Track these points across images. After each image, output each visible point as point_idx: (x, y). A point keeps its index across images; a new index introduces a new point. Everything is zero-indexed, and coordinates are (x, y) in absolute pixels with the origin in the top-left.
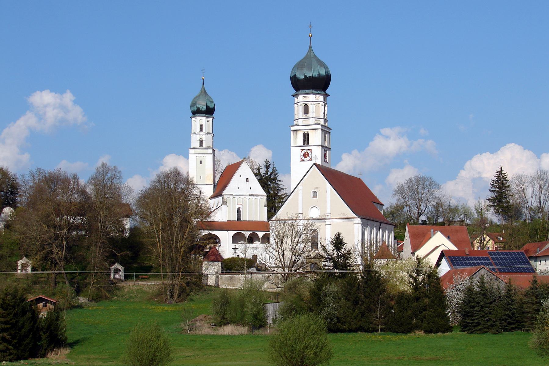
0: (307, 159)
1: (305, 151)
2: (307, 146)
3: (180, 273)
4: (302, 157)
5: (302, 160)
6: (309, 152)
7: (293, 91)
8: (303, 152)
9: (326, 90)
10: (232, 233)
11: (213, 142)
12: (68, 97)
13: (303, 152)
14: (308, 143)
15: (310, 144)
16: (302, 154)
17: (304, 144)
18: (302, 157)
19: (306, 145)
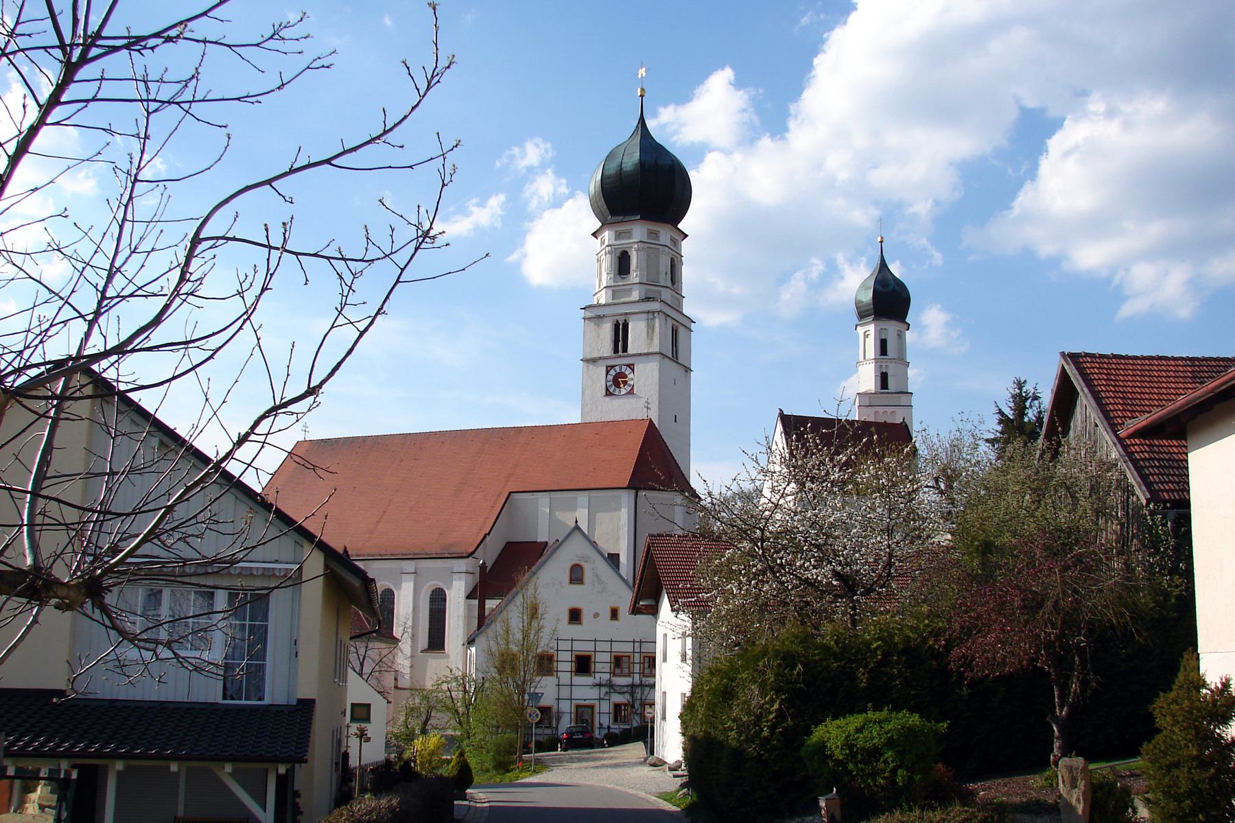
0: (623, 391)
1: (618, 369)
2: (624, 357)
3: (1058, 543)
4: (609, 384)
5: (608, 393)
6: (628, 371)
7: (857, 321)
8: (612, 372)
9: (169, 428)
10: (560, 541)
11: (405, 117)
12: (549, 145)
13: (612, 372)
14: (625, 349)
15: (631, 350)
16: (610, 378)
17: (616, 351)
18: (609, 384)
19: (620, 353)
